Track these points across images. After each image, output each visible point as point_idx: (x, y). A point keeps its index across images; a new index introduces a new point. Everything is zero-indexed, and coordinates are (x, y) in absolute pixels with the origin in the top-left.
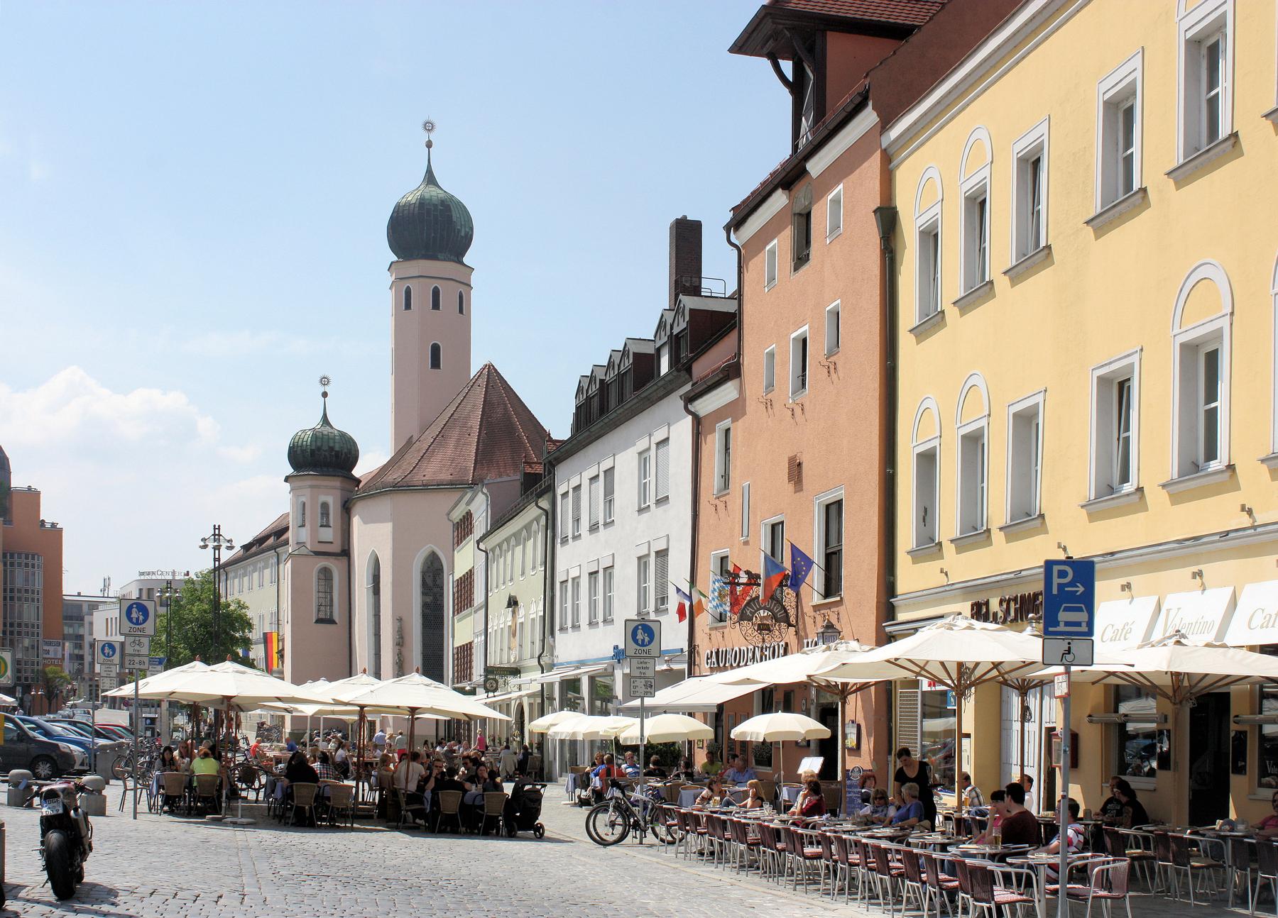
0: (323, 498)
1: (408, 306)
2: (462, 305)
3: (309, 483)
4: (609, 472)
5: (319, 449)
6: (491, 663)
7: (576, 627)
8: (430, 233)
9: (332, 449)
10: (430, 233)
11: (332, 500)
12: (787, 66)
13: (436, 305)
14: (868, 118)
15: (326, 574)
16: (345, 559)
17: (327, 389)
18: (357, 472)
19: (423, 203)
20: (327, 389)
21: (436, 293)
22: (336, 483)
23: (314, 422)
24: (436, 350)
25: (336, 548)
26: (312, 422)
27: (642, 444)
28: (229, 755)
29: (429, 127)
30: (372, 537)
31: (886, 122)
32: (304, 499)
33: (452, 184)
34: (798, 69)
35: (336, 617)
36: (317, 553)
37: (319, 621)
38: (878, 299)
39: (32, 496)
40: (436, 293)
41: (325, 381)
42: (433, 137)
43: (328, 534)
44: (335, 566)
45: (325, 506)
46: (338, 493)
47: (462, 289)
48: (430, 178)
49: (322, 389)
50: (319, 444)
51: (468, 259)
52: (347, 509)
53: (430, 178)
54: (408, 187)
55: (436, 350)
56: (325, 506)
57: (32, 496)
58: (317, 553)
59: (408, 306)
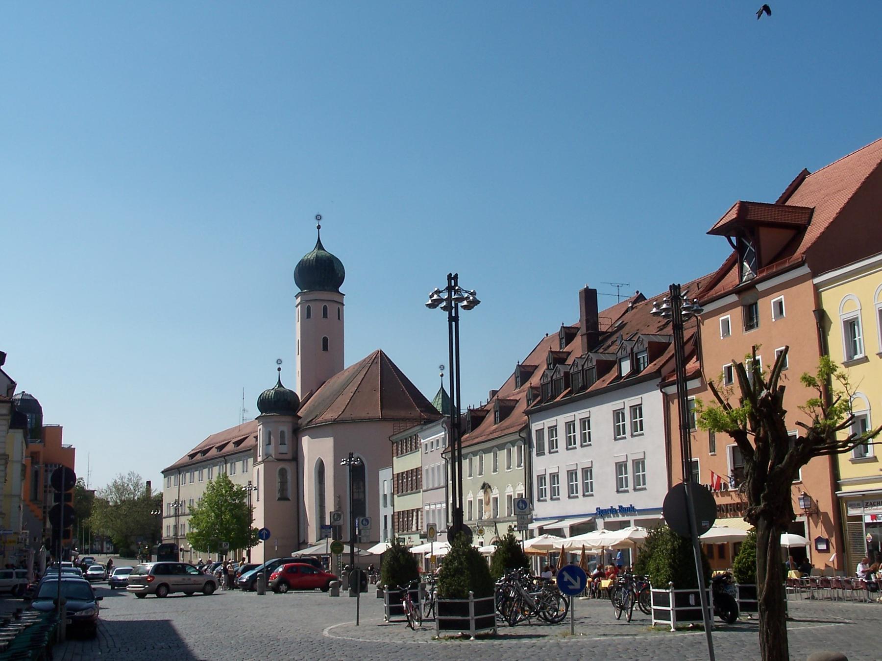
1: (309, 316)
2: (340, 316)
4: (586, 423)
8: (321, 276)
10: (321, 276)
11: (286, 428)
12: (734, 239)
13: (325, 315)
14: (805, 270)
15: (283, 473)
16: (294, 463)
18: (299, 414)
19: (318, 259)
21: (325, 308)
22: (288, 419)
23: (273, 384)
24: (325, 340)
25: (289, 456)
27: (617, 405)
28: (535, 582)
29: (319, 218)
30: (316, 450)
31: (815, 274)
33: (331, 248)
34: (738, 241)
36: (279, 460)
38: (818, 349)
39: (57, 431)
40: (325, 308)
41: (279, 362)
43: (284, 449)
44: (289, 468)
45: (282, 433)
47: (337, 306)
48: (319, 245)
51: (341, 289)
52: (297, 432)
53: (319, 245)
54: (306, 251)
55: (325, 340)
56: (282, 433)
57: (57, 431)
58: (279, 460)
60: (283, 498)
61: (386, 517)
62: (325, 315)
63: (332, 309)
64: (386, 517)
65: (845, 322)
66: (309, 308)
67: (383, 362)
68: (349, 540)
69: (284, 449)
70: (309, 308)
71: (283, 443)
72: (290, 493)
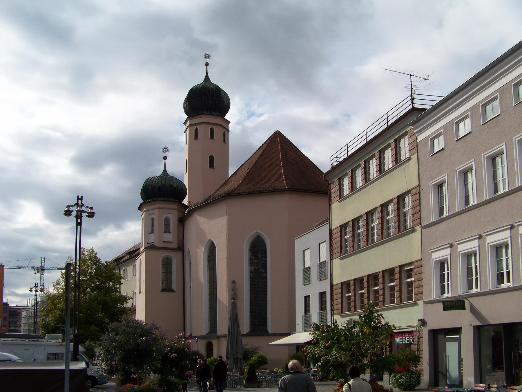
0: (165, 216)
1: (196, 137)
3: (157, 206)
5: (164, 186)
6: (456, 344)
7: (392, 302)
9: (171, 186)
11: (173, 217)
13: (212, 136)
15: (167, 264)
17: (167, 154)
20: (167, 154)
21: (212, 131)
22: (175, 206)
23: (160, 172)
24: (212, 159)
25: (175, 245)
26: (199, 80)
29: (207, 56)
32: (153, 216)
35: (174, 287)
37: (163, 290)
40: (212, 131)
42: (209, 61)
43: (169, 237)
44: (175, 258)
45: (167, 220)
46: (176, 212)
48: (207, 77)
49: (163, 155)
50: (163, 183)
51: (227, 117)
52: (182, 221)
55: (212, 159)
56: (167, 220)
59: (196, 137)
60: (167, 289)
61: (307, 299)
62: (212, 136)
63: (218, 131)
64: (307, 299)
65: (444, 310)
66: (197, 131)
67: (278, 143)
68: (416, 106)
69: (169, 237)
70: (197, 131)
71: (167, 231)
72: (175, 285)
